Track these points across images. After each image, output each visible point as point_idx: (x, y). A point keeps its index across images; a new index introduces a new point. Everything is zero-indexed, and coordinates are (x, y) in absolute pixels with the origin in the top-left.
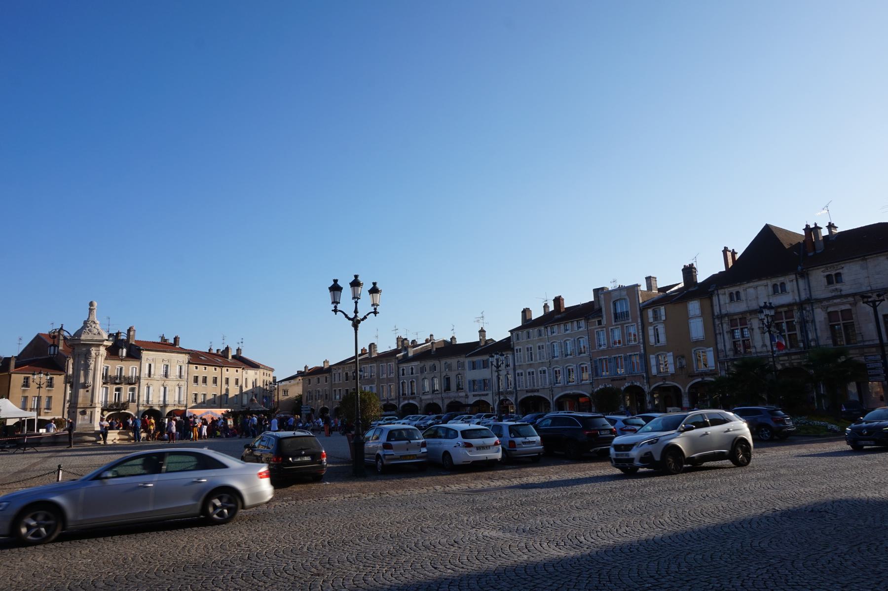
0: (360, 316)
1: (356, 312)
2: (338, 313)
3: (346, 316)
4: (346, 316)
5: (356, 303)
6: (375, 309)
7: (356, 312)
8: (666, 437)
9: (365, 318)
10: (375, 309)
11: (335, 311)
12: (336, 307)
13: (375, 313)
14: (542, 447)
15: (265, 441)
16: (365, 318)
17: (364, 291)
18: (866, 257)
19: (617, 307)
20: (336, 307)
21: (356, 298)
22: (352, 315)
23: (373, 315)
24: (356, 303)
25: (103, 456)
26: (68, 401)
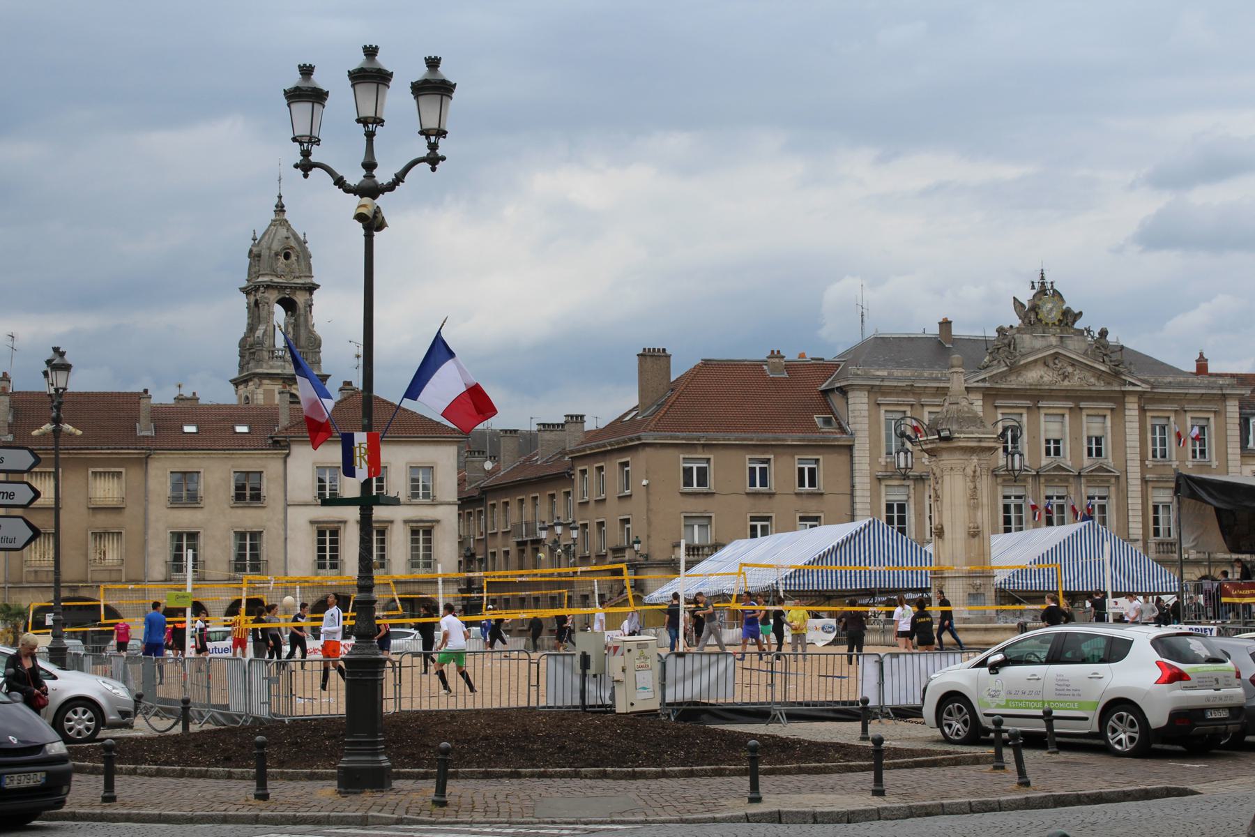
0: (383, 175)
1: (370, 166)
2: (315, 172)
3: (340, 182)
4: (340, 182)
5: (370, 136)
6: (433, 147)
7: (370, 166)
8: (545, 685)
9: (399, 179)
10: (433, 147)
11: (306, 166)
12: (306, 154)
13: (433, 160)
14: (103, 765)
15: (481, 739)
16: (399, 179)
17: (397, 99)
18: (1082, 405)
19: (603, 574)
20: (306, 154)
21: (370, 124)
22: (355, 177)
23: (426, 166)
24: (370, 136)
25: (242, 686)
26: (633, 770)
